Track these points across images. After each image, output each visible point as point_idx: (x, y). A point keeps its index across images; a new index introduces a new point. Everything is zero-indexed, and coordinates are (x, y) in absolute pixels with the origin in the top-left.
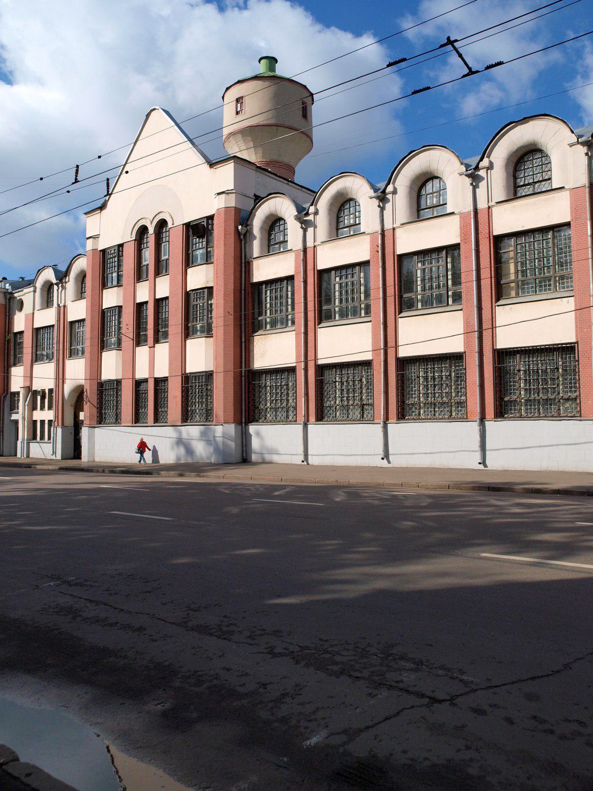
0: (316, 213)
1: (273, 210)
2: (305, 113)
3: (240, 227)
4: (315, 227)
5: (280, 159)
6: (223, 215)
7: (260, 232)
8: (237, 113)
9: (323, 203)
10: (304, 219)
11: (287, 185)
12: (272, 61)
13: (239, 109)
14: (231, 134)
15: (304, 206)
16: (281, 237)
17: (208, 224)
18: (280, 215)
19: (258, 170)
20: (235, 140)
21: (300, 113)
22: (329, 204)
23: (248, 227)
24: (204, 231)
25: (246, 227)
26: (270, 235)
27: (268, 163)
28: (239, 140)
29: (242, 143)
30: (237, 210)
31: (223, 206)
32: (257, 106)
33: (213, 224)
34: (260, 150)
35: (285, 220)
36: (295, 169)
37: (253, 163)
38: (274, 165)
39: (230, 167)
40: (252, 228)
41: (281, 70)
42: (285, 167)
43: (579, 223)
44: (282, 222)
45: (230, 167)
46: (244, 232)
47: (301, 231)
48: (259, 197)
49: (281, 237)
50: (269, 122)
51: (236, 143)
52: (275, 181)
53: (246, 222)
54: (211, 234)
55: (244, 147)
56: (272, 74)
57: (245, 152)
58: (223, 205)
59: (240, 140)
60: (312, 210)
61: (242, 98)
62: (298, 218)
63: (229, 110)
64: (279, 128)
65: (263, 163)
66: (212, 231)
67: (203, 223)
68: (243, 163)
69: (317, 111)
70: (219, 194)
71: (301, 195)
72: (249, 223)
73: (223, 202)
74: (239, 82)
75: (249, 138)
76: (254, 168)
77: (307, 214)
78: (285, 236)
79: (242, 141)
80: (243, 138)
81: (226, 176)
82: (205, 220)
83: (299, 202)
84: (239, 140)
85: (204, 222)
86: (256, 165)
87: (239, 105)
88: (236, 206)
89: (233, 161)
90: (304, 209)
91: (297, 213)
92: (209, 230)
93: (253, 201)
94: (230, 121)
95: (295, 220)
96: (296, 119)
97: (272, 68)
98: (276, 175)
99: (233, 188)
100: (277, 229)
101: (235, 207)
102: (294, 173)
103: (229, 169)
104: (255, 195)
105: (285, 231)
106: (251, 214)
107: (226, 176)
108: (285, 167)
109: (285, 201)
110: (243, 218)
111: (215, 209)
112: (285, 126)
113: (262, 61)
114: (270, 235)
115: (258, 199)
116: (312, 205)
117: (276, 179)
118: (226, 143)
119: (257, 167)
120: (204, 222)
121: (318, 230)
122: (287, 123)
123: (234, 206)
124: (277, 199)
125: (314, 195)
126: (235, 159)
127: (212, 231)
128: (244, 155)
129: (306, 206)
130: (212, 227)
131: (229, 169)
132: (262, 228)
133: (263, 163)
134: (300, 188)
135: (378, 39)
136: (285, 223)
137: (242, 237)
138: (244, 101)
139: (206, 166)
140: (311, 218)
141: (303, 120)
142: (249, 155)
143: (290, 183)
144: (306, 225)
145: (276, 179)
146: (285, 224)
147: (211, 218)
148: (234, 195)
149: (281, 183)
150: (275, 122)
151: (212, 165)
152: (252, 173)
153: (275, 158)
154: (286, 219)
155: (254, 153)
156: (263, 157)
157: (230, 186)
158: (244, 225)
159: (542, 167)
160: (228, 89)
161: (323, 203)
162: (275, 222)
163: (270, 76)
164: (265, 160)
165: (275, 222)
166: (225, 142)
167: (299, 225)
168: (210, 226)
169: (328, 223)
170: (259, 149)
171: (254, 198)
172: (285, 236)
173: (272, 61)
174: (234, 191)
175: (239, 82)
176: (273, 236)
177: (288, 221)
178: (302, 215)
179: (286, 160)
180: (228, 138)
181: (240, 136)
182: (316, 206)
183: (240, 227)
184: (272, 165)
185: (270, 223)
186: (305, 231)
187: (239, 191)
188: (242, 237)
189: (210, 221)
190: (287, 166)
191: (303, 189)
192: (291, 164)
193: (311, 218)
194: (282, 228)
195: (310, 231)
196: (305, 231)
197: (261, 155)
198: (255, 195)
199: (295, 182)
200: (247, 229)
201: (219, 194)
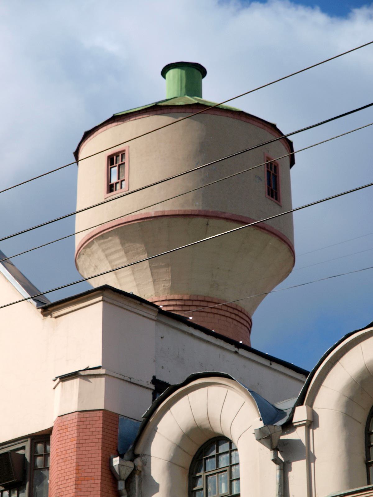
0: (312, 423)
1: (200, 416)
2: (274, 185)
3: (116, 461)
4: (311, 459)
5: (215, 294)
6: (73, 432)
7: (167, 474)
8: (111, 188)
9: (330, 397)
10: (282, 438)
11: (235, 357)
12: (194, 72)
13: (114, 180)
14: (101, 236)
15: (281, 406)
16: (223, 485)
17: (34, 454)
18: (218, 430)
19: (164, 319)
20: (104, 251)
21: (262, 187)
22: (344, 399)
23: (138, 461)
24: (24, 471)
25: (132, 460)
26: (193, 479)
27: (186, 304)
28: (113, 250)
29: (120, 258)
30: (110, 418)
31: (74, 407)
32: (159, 169)
33: (46, 455)
34: (166, 276)
35: (231, 442)
36: (253, 318)
37: (152, 304)
38: (199, 309)
39: (93, 314)
40: (147, 464)
41: (212, 92)
42: (228, 314)
43: (87, 423)
44: (224, 447)
45: (93, 314)
46: (125, 473)
47: (274, 470)
48: (166, 385)
49: (223, 485)
50: (188, 208)
51: (107, 256)
52: (204, 346)
53: (131, 447)
54: (42, 479)
55: (124, 261)
56: (193, 100)
57: (127, 272)
58: (73, 406)
59: (116, 252)
60: (301, 414)
61: (122, 154)
62: (266, 437)
63: (91, 175)
64: (212, 222)
65: (174, 303)
66: (45, 472)
67: (21, 452)
68: (122, 301)
69: (303, 181)
70: (64, 378)
71: (271, 380)
72: (139, 450)
73: (75, 398)
74: (116, 119)
75: (140, 247)
76: (153, 314)
77: (289, 426)
78: (231, 481)
79: (122, 253)
80: (123, 244)
81: (83, 334)
82: (28, 444)
83: (268, 396)
84: (113, 250)
85: (23, 448)
86: (157, 307)
87: (115, 170)
88: (107, 409)
89: (100, 298)
90: (280, 413)
91: (261, 424)
92: (35, 468)
93: (149, 395)
94: (93, 207)
95: (259, 440)
96: (257, 205)
97: (193, 88)
98: (208, 332)
99: (99, 364)
100: (210, 464)
101: (104, 411)
102: (249, 326)
103: (89, 320)
104: (155, 381)
105: (233, 469)
106: (145, 427)
107: (83, 334)
108: (228, 314)
109: (230, 392)
110: (124, 437)
111: (55, 417)
112: (226, 215)
113: (171, 73)
114: (193, 479)
115: (163, 392)
116: (300, 402)
117: (208, 342)
118: (83, 258)
119: (161, 312)
120: (23, 448)
121: (319, 467)
122: (231, 210)
123: (103, 408)
124: (212, 389)
125: (307, 380)
126: (106, 293)
127: (45, 472)
128: (126, 282)
129: (285, 405)
130: (46, 461)
131: (89, 320)
132: (172, 464)
133: (174, 303)
134: (267, 363)
135: (366, 364)
136: (232, 450)
137: (121, 486)
138: (126, 160)
139: (30, 309)
140: (298, 434)
141: (270, 203)
142: (137, 285)
143: (241, 351)
144: (285, 453)
145: (208, 342)
146: (231, 451)
147: (42, 438)
148: (103, 380)
149: (219, 351)
150: (201, 208)
151: (47, 309)
152: (148, 328)
153: (203, 291)
154: (234, 439)
155: (151, 280)
156: (173, 289)
157: (94, 358)
158: (126, 456)
159: (231, 456)
160: (87, 135)
161: (330, 397)
162: (206, 448)
163: (188, 102)
164: (176, 297)
165: (206, 448)
166: (79, 255)
167: (268, 454)
168: (39, 460)
169: (343, 447)
170: (164, 270)
171: (153, 387)
172: (231, 481)
173: (194, 72)
174: (102, 371)
175: (116, 119)
176: (200, 484)
177: (239, 444)
178: (276, 428)
179: (229, 296)
180: (89, 246)
181: (117, 240)
182: (310, 405)
183: (116, 461)
184: (194, 309)
185: (193, 450)
186: (285, 469)
187: (113, 369)
188: (121, 486)
189: (40, 446)
190: (231, 310)
191: (275, 366)
192: (243, 304)
193: (298, 434)
194: (224, 462)
195: (298, 468)
196: (285, 469)
197: (168, 284)
198: (155, 381)
199: (253, 346)
200: (135, 467)
201: (64, 378)
